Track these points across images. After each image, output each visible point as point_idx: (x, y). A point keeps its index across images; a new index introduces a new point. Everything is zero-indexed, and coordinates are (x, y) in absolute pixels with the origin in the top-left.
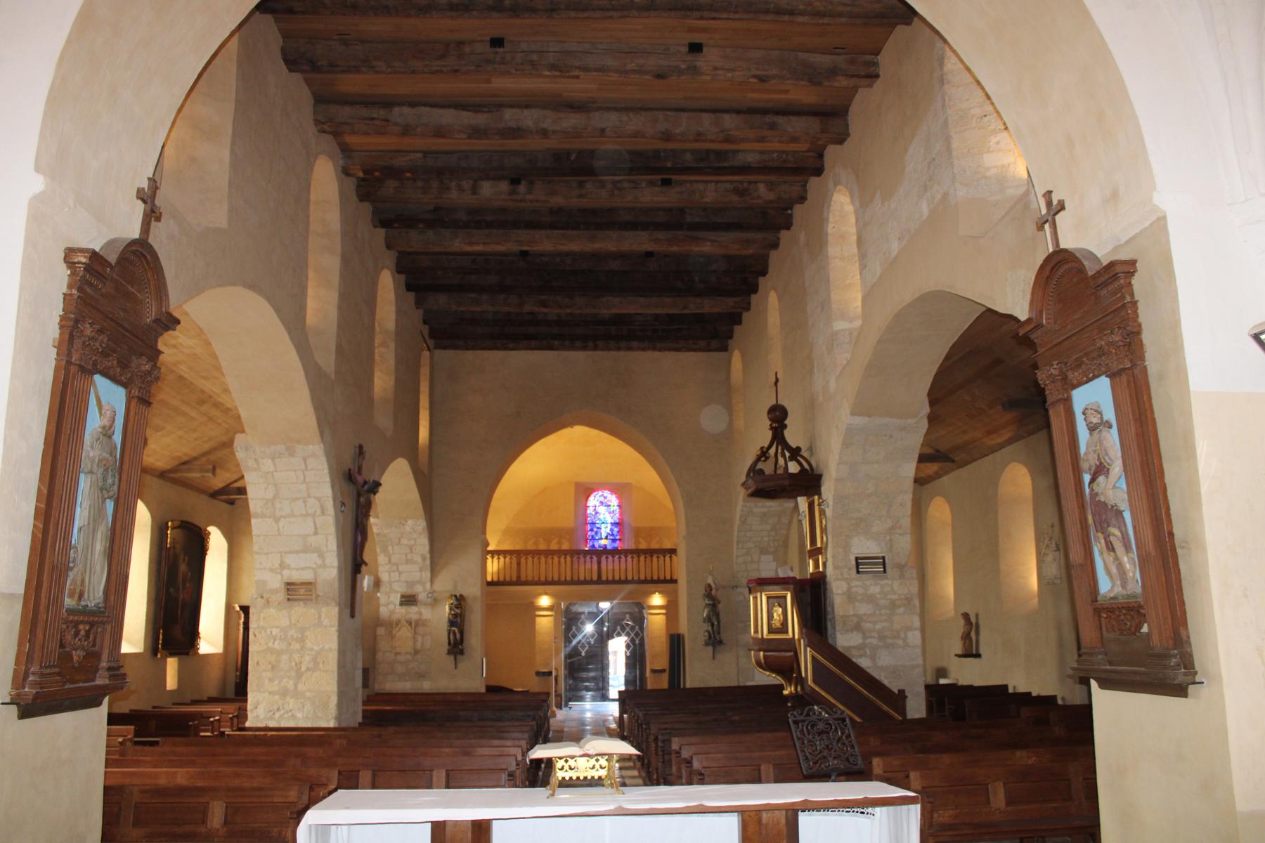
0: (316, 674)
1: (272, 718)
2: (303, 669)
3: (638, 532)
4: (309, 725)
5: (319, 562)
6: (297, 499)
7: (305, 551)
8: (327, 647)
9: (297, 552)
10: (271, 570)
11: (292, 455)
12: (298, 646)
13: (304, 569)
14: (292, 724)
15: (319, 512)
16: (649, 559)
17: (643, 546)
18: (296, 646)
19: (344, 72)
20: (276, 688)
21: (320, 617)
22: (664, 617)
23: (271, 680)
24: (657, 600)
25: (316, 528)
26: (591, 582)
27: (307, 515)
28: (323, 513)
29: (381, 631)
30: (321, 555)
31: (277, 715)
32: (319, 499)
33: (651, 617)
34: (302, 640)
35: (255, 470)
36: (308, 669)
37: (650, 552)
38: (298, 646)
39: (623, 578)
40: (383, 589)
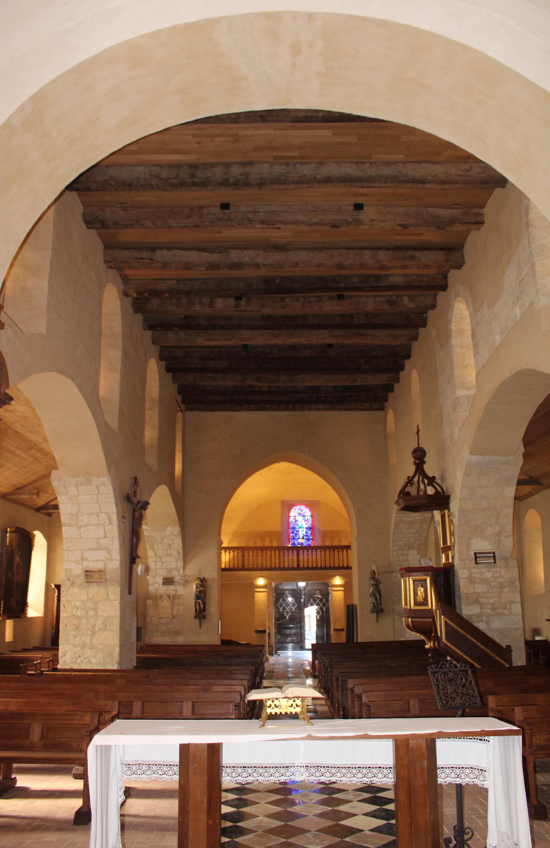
1: (75, 663)
2: (96, 629)
3: (324, 534)
5: (108, 556)
6: (93, 514)
8: (112, 614)
9: (92, 550)
10: (75, 562)
11: (89, 484)
15: (107, 523)
17: (328, 543)
18: (91, 613)
20: (78, 642)
21: (108, 594)
22: (342, 593)
23: (75, 637)
24: (338, 581)
25: (105, 533)
27: (100, 525)
28: (110, 523)
29: (149, 602)
31: (79, 660)
32: (107, 514)
33: (334, 593)
34: (95, 610)
36: (100, 629)
37: (333, 548)
39: (323, 566)
40: (150, 574)
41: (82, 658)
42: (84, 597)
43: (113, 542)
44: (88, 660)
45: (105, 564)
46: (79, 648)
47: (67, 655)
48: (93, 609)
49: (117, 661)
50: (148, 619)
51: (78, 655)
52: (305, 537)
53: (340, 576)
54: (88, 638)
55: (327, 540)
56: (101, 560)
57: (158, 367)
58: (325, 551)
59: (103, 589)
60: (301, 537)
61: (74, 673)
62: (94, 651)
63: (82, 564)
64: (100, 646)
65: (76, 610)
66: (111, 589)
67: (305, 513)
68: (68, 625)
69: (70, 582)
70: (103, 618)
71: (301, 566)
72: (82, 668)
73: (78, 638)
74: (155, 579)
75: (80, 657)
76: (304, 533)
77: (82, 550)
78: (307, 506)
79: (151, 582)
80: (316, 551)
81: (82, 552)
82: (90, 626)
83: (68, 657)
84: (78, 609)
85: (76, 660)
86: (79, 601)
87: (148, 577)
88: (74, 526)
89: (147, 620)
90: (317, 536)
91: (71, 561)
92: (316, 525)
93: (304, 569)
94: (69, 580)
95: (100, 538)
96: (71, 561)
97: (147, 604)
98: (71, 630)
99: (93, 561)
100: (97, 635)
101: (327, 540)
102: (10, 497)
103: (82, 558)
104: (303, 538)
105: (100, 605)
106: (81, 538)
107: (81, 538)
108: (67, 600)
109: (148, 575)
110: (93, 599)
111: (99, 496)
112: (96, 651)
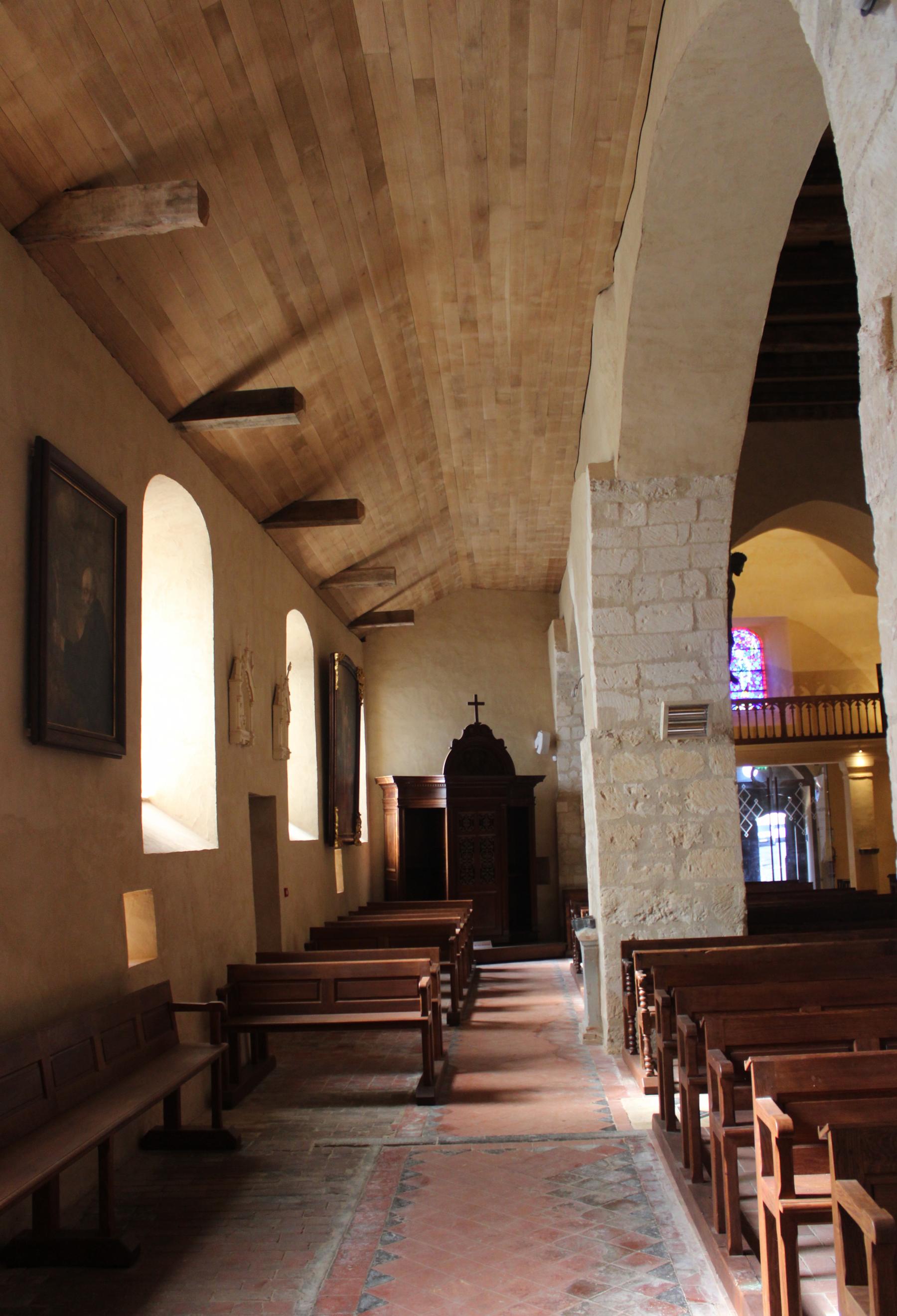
0: (706, 853)
1: (640, 926)
2: (686, 846)
3: (798, 678)
4: (704, 935)
5: (700, 675)
6: (672, 572)
7: (676, 659)
8: (721, 809)
9: (663, 661)
10: (623, 691)
11: (681, 495)
12: (674, 810)
13: (674, 687)
14: (674, 934)
15: (702, 593)
16: (830, 708)
17: (806, 693)
18: (671, 810)
19: (268, 274)
20: (644, 878)
21: (706, 762)
22: (869, 782)
23: (636, 866)
24: (860, 760)
25: (695, 620)
26: (774, 740)
27: (682, 600)
28: (709, 594)
29: (562, 807)
30: (702, 665)
31: (650, 920)
32: (705, 572)
33: (852, 782)
34: (681, 799)
35: (613, 524)
36: (694, 846)
37: (814, 701)
38: (674, 810)
39: (815, 733)
40: (561, 750)
41: (658, 915)
42: (650, 773)
43: (712, 641)
44: (671, 918)
45: (694, 693)
46: (647, 892)
47: (620, 908)
48: (672, 801)
49: (742, 917)
50: (562, 840)
51: (647, 909)
52: (750, 688)
53: (864, 750)
54: (668, 868)
55: (803, 689)
56: (686, 684)
57: (119, 501)
58: (800, 706)
59: (693, 752)
60: (743, 688)
61: (709, 949)
62: (685, 896)
63: (638, 696)
64: (697, 884)
65: (632, 804)
66: (712, 751)
67: (749, 642)
68: (616, 840)
69: (612, 741)
70: (701, 819)
71: (790, 734)
72: (660, 937)
73: (645, 868)
74: (570, 761)
75: (651, 912)
76: (748, 680)
77: (638, 662)
78: (750, 630)
79: (560, 767)
80: (800, 706)
81: (638, 668)
82: (670, 838)
83: (624, 914)
84: (637, 803)
85: (644, 919)
86: (639, 782)
87: (554, 758)
88: (622, 605)
89: (560, 842)
90: (776, 684)
91: (612, 689)
92: (775, 664)
93: (794, 739)
94: (610, 735)
95: (682, 633)
96: (612, 689)
97: (558, 810)
98: (624, 851)
99: (665, 689)
100: (688, 859)
101: (803, 689)
102: (366, 566)
103: (637, 682)
104: (747, 690)
105: (689, 789)
106: (636, 633)
107: (636, 633)
108: (608, 783)
109: (555, 755)
110: (673, 777)
111: (694, 526)
112: (689, 896)
